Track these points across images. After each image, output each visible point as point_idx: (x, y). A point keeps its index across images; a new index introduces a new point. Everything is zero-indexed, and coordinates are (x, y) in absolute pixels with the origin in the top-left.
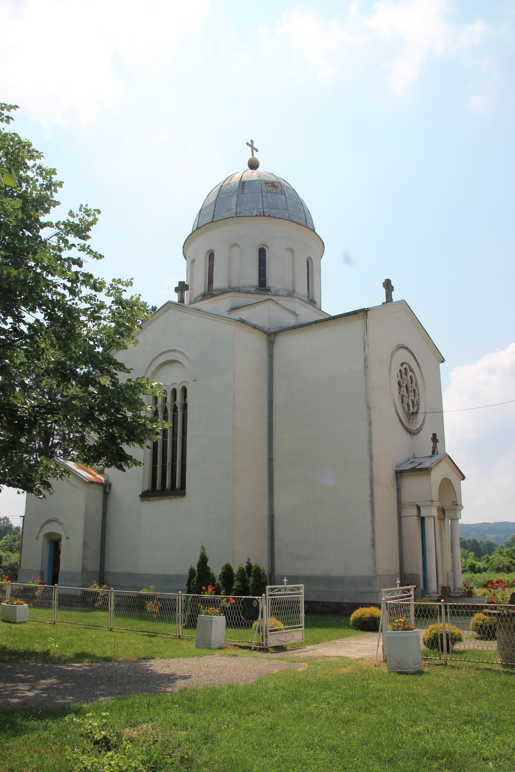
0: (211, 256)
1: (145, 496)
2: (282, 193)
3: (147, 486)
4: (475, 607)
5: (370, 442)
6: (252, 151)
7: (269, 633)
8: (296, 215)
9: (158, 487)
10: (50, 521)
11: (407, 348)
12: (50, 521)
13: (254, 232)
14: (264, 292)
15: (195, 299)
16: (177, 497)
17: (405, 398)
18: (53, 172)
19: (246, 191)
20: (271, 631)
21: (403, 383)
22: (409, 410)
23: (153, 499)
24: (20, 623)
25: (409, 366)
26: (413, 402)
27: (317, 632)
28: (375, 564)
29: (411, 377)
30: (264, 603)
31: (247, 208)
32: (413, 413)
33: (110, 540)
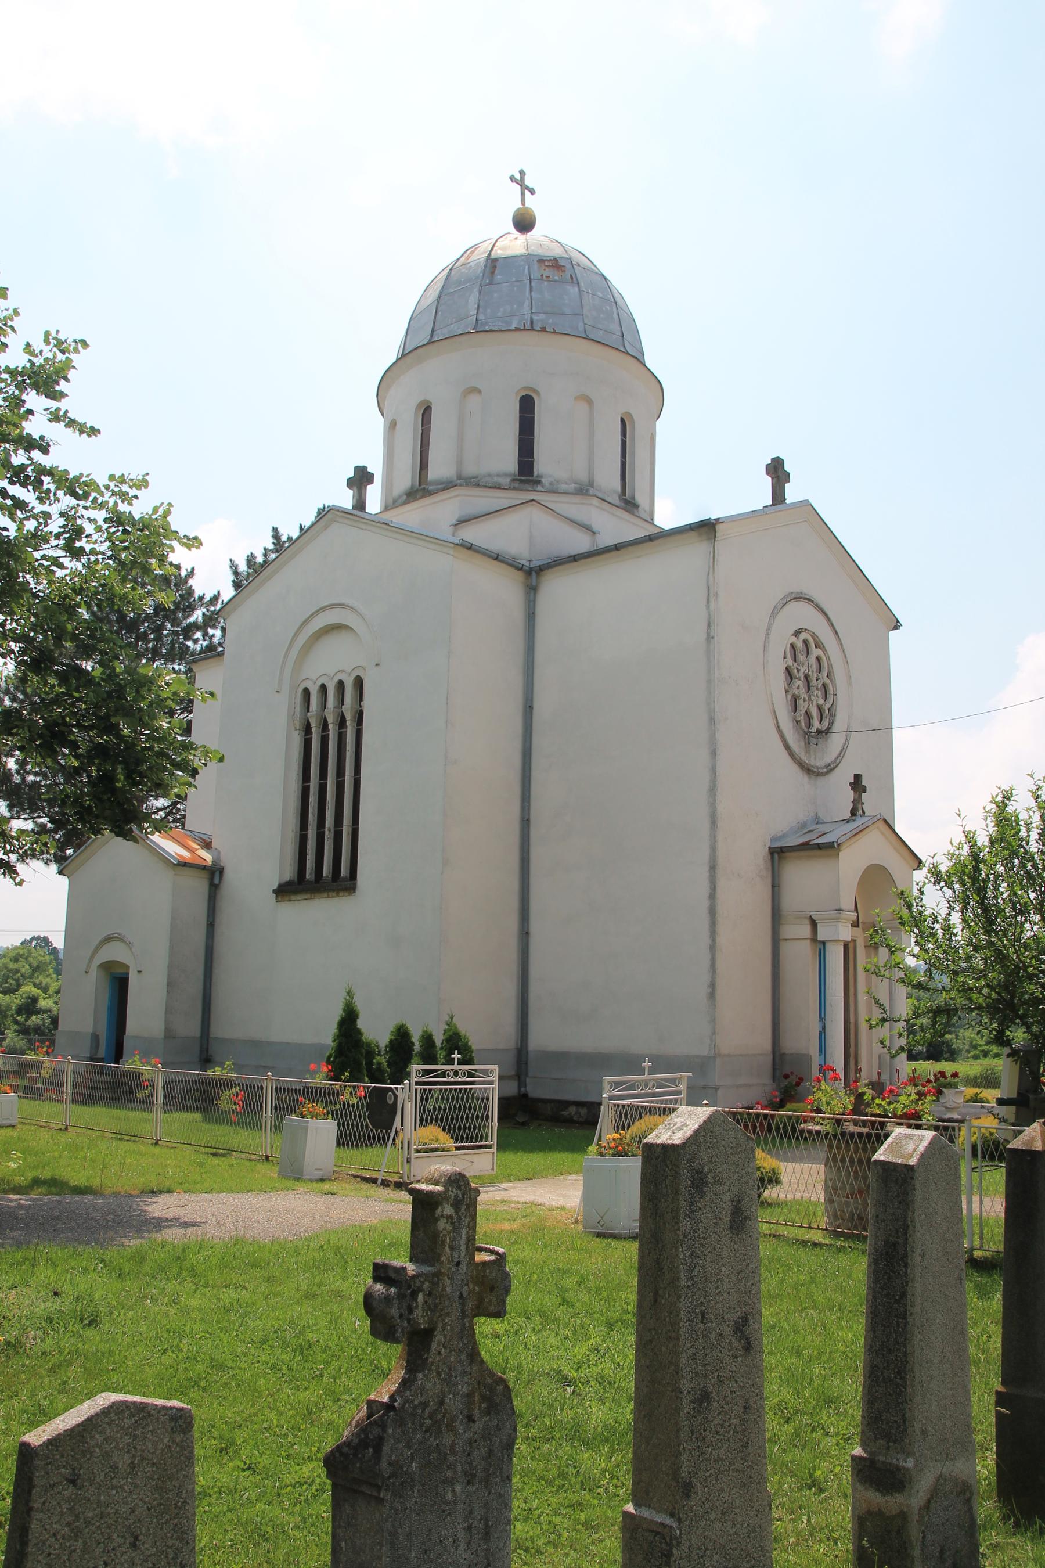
0: (426, 412)
1: (284, 891)
2: (574, 280)
3: (289, 873)
4: (761, 1117)
5: (713, 790)
6: (523, 194)
7: (414, 1155)
8: (600, 326)
9: (309, 874)
10: (108, 939)
11: (809, 600)
12: (108, 939)
14: (527, 486)
15: (395, 501)
16: (341, 894)
17: (802, 701)
19: (498, 277)
20: (418, 1151)
21: (798, 670)
22: (810, 725)
23: (299, 897)
25: (814, 636)
26: (820, 709)
27: (517, 1159)
28: (714, 1033)
29: (818, 659)
30: (406, 1096)
31: (499, 314)
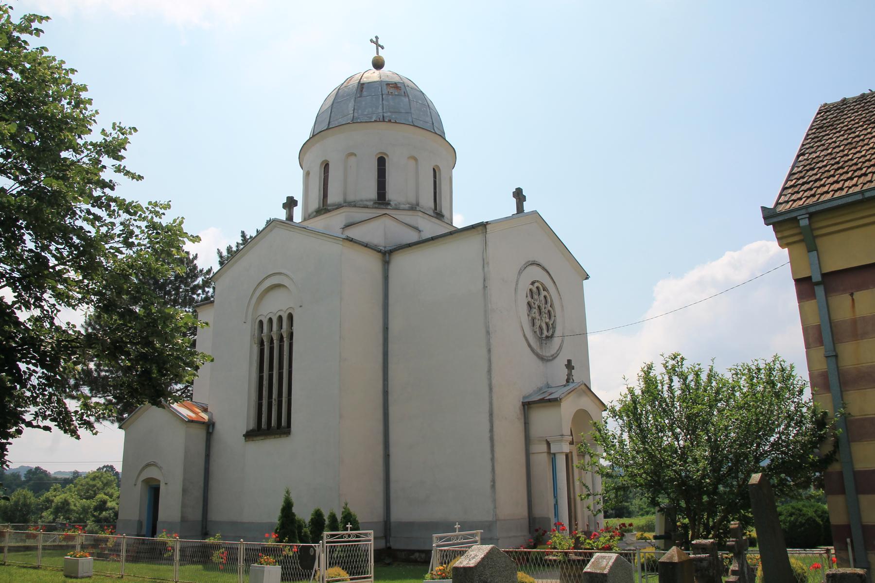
0: (326, 166)
1: (250, 435)
2: (406, 94)
3: (252, 425)
5: (489, 371)
10: (148, 465)
12: (148, 465)
13: (370, 140)
18: (85, 88)
19: (365, 93)
22: (542, 333)
23: (258, 438)
24: (82, 577)
25: (542, 284)
26: (547, 324)
28: (495, 508)
29: (545, 297)
32: (547, 337)
33: (214, 484)
